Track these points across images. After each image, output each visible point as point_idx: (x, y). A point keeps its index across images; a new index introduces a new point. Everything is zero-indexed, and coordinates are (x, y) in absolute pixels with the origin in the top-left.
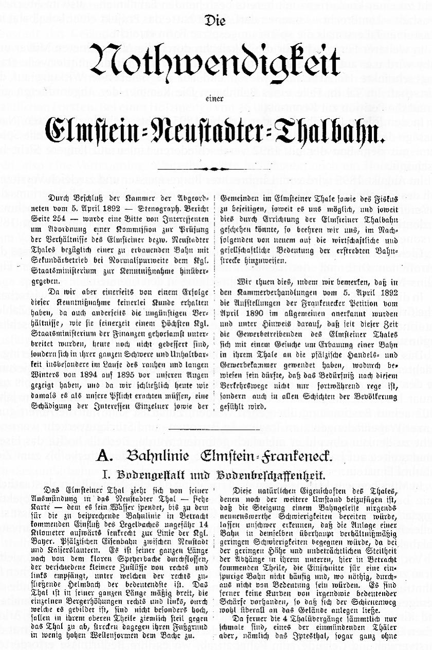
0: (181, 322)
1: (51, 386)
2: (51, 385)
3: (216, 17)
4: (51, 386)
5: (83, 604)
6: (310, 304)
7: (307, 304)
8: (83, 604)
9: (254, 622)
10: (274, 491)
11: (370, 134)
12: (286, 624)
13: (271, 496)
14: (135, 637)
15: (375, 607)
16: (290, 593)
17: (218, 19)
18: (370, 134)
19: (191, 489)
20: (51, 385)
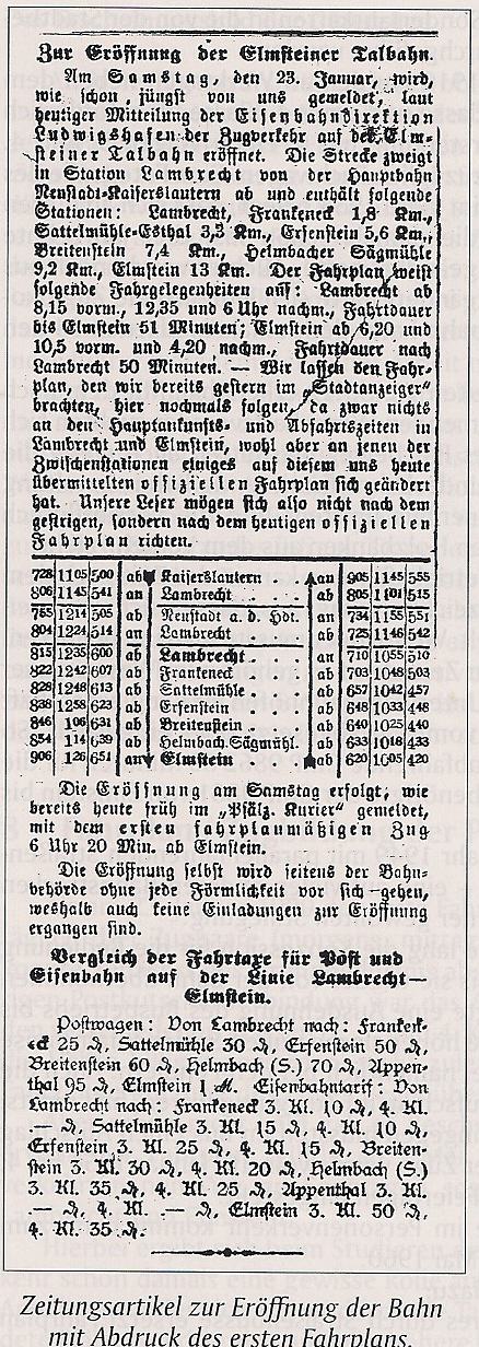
0: (206, 706)
1: (426, 160)
2: (426, 157)
3: (75, 785)
4: (426, 160)
5: (399, 201)
6: (270, 215)
7: (264, 216)
8: (399, 201)
9: (398, 819)
10: (301, 960)
11: (301, 1254)
12: (229, 320)
13: (309, 883)
14: (308, 527)
15: (226, 586)
16: (405, 334)
17: (77, 787)
18: (301, 1254)
19: (189, 868)
20: (426, 157)
